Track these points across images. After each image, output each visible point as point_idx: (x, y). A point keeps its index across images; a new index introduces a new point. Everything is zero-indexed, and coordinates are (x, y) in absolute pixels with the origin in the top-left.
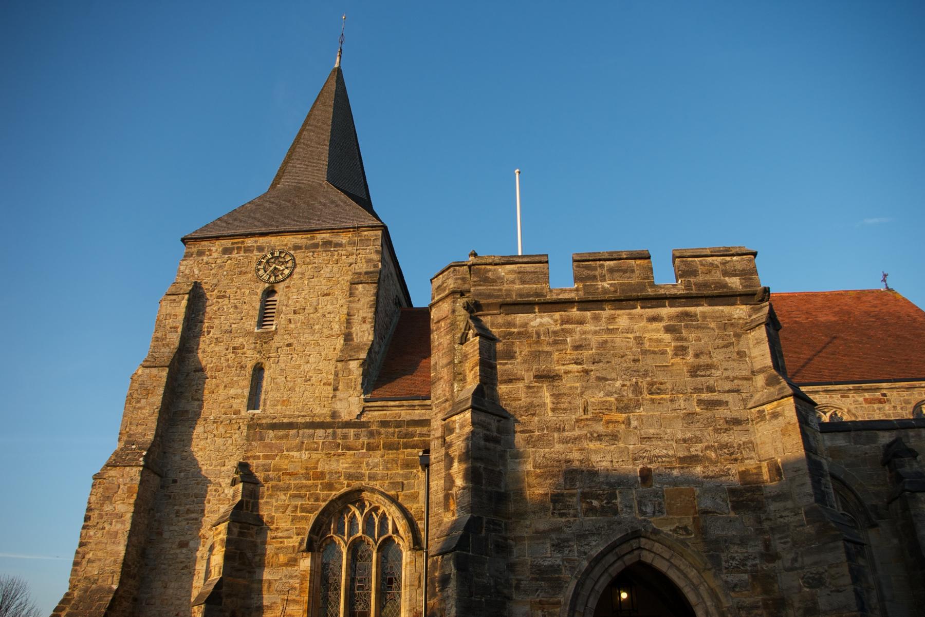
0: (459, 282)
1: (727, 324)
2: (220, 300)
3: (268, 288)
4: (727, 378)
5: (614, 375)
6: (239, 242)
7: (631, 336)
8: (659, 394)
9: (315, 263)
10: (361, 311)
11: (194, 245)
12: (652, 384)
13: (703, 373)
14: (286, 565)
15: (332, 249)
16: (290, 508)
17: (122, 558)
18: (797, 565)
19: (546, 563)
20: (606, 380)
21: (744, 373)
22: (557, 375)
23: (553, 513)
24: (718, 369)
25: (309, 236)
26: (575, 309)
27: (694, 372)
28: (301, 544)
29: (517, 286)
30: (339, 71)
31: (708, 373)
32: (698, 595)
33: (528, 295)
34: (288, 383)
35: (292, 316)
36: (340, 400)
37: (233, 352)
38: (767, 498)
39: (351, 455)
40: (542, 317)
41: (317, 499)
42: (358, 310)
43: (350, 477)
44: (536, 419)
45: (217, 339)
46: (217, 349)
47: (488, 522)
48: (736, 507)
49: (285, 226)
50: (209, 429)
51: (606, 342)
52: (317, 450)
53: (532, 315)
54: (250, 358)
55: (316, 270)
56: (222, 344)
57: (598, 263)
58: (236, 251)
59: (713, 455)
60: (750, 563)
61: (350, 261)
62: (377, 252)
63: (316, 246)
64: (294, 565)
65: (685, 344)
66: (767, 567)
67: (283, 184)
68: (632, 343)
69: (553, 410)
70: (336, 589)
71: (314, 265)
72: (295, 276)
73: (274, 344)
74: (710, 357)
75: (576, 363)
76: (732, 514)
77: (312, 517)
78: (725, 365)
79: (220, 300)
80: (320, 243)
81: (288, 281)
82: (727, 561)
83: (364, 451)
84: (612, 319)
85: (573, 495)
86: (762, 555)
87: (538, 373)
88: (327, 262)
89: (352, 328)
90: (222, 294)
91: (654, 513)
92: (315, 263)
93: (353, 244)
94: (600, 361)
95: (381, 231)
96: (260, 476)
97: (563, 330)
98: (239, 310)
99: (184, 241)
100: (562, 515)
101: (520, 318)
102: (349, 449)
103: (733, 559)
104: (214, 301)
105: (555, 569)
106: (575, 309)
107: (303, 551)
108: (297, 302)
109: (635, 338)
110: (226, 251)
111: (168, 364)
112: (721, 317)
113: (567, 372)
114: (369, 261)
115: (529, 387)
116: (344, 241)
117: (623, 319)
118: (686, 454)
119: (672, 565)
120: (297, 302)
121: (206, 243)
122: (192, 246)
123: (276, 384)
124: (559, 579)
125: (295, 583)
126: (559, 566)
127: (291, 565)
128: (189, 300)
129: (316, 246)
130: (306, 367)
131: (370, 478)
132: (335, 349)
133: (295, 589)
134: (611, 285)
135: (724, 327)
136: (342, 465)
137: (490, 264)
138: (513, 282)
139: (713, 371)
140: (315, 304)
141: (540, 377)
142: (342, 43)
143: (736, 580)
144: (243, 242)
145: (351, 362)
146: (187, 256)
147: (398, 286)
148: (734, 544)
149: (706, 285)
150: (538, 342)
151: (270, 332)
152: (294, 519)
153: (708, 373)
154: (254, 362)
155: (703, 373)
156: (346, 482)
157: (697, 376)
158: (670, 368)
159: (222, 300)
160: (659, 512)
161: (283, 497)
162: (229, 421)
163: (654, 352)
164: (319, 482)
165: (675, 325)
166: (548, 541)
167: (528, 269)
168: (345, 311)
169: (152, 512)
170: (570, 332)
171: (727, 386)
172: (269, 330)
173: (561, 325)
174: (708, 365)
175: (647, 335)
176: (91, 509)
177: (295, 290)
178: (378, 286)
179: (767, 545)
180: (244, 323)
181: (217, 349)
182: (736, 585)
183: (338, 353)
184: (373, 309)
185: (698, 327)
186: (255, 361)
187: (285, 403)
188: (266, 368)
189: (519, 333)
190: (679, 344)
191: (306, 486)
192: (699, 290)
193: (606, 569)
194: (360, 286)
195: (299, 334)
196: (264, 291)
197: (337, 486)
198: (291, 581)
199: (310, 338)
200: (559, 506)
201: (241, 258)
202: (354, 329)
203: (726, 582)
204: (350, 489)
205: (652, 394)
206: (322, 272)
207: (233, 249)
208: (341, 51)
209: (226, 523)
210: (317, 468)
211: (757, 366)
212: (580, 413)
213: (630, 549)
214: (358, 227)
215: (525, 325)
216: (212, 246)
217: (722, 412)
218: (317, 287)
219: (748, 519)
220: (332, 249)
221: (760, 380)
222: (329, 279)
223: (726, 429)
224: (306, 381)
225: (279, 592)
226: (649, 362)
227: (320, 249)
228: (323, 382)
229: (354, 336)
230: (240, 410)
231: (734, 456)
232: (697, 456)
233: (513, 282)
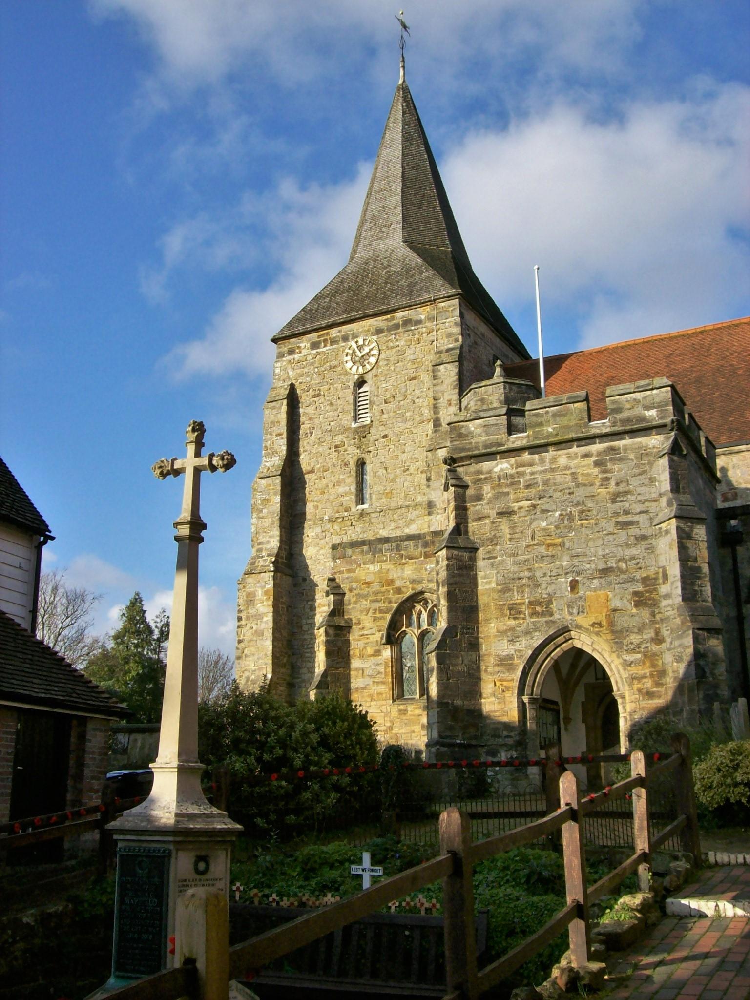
0: (479, 403)
1: (644, 454)
2: (316, 399)
3: (358, 379)
4: (640, 501)
5: (554, 507)
6: (324, 334)
8: (587, 519)
9: (398, 346)
10: (445, 394)
11: (284, 343)
12: (582, 512)
13: (621, 499)
14: (373, 655)
15: (413, 328)
17: (271, 652)
18: (672, 647)
19: (504, 654)
20: (548, 511)
21: (654, 496)
22: (513, 511)
23: (509, 618)
24: (633, 494)
25: (389, 316)
26: (527, 453)
27: (615, 497)
28: (382, 638)
29: (483, 439)
30: (405, 90)
31: (625, 498)
33: (491, 445)
34: (389, 475)
35: (384, 406)
36: (434, 490)
37: (335, 451)
38: (660, 596)
39: (412, 563)
40: (502, 464)
41: (390, 602)
42: (443, 392)
43: (413, 581)
44: (498, 548)
46: (321, 449)
47: (463, 628)
48: (636, 606)
49: (365, 310)
50: (326, 528)
51: (549, 480)
52: (386, 561)
53: (495, 462)
54: (352, 454)
55: (401, 353)
56: (324, 444)
57: (545, 410)
58: (323, 344)
59: (624, 566)
60: (643, 646)
61: (432, 338)
62: (456, 324)
63: (397, 326)
64: (379, 656)
65: (609, 475)
66: (655, 648)
67: (360, 254)
69: (510, 539)
71: (398, 348)
72: (381, 363)
73: (371, 438)
74: (628, 485)
75: (527, 500)
76: (634, 610)
77: (388, 617)
78: (639, 490)
79: (315, 399)
80: (401, 323)
81: (374, 370)
82: (627, 646)
83: (423, 558)
84: (554, 460)
85: (524, 603)
86: (652, 639)
87: (500, 511)
89: (439, 413)
90: (317, 392)
91: (578, 613)
92: (398, 346)
93: (431, 319)
95: (458, 300)
97: (517, 473)
98: (335, 407)
99: (275, 340)
100: (515, 619)
101: (486, 465)
102: (411, 558)
103: (632, 643)
104: (311, 400)
105: (510, 657)
106: (527, 453)
107: (384, 644)
108: (386, 390)
110: (315, 345)
111: (279, 472)
112: (640, 448)
113: (520, 508)
114: (449, 335)
115: (493, 523)
116: (423, 317)
117: (562, 457)
118: (604, 566)
120: (386, 390)
121: (294, 340)
122: (283, 346)
125: (381, 668)
126: (512, 655)
127: (377, 656)
128: (288, 405)
129: (397, 326)
130: (403, 457)
131: (429, 581)
132: (427, 434)
134: (554, 429)
135: (641, 457)
136: (409, 571)
137: (463, 421)
138: (480, 435)
139: (629, 496)
140: (404, 390)
141: (500, 514)
142: (402, 48)
143: (632, 659)
144: (328, 334)
145: (439, 451)
146: (281, 356)
148: (633, 633)
149: (628, 420)
150: (499, 485)
151: (366, 425)
153: (625, 498)
154: (355, 458)
155: (621, 499)
156: (411, 586)
157: (616, 502)
158: (596, 497)
159: (318, 398)
160: (582, 612)
161: (365, 603)
162: (341, 519)
163: (585, 485)
165: (602, 460)
166: (506, 638)
167: (491, 423)
168: (431, 394)
169: (290, 609)
170: (522, 474)
171: (638, 508)
172: (365, 423)
173: (516, 468)
174: (625, 492)
176: (241, 611)
177: (383, 379)
178: (460, 364)
179: (657, 632)
180: (341, 420)
181: (321, 449)
182: (632, 662)
183: (425, 442)
184: (457, 390)
185: (621, 459)
186: (356, 457)
187: (389, 495)
188: (368, 462)
189: (486, 479)
190: (605, 475)
192: (623, 426)
194: (442, 366)
195: (393, 423)
196: (355, 383)
197: (404, 590)
198: (378, 667)
200: (513, 612)
201: (329, 351)
202: (441, 413)
203: (625, 660)
204: (414, 592)
205: (582, 520)
206: (406, 355)
207: (319, 342)
208: (403, 61)
209: (324, 628)
211: (663, 491)
212: (529, 541)
213: (564, 640)
214: (435, 300)
215: (490, 472)
216: (300, 343)
217: (634, 531)
218: (403, 372)
219: (645, 614)
220: (413, 328)
223: (636, 544)
224: (404, 471)
225: (370, 676)
226: (581, 493)
227: (401, 330)
228: (420, 470)
229: (442, 420)
230: (350, 508)
231: (639, 566)
232: (612, 568)
233: (480, 435)
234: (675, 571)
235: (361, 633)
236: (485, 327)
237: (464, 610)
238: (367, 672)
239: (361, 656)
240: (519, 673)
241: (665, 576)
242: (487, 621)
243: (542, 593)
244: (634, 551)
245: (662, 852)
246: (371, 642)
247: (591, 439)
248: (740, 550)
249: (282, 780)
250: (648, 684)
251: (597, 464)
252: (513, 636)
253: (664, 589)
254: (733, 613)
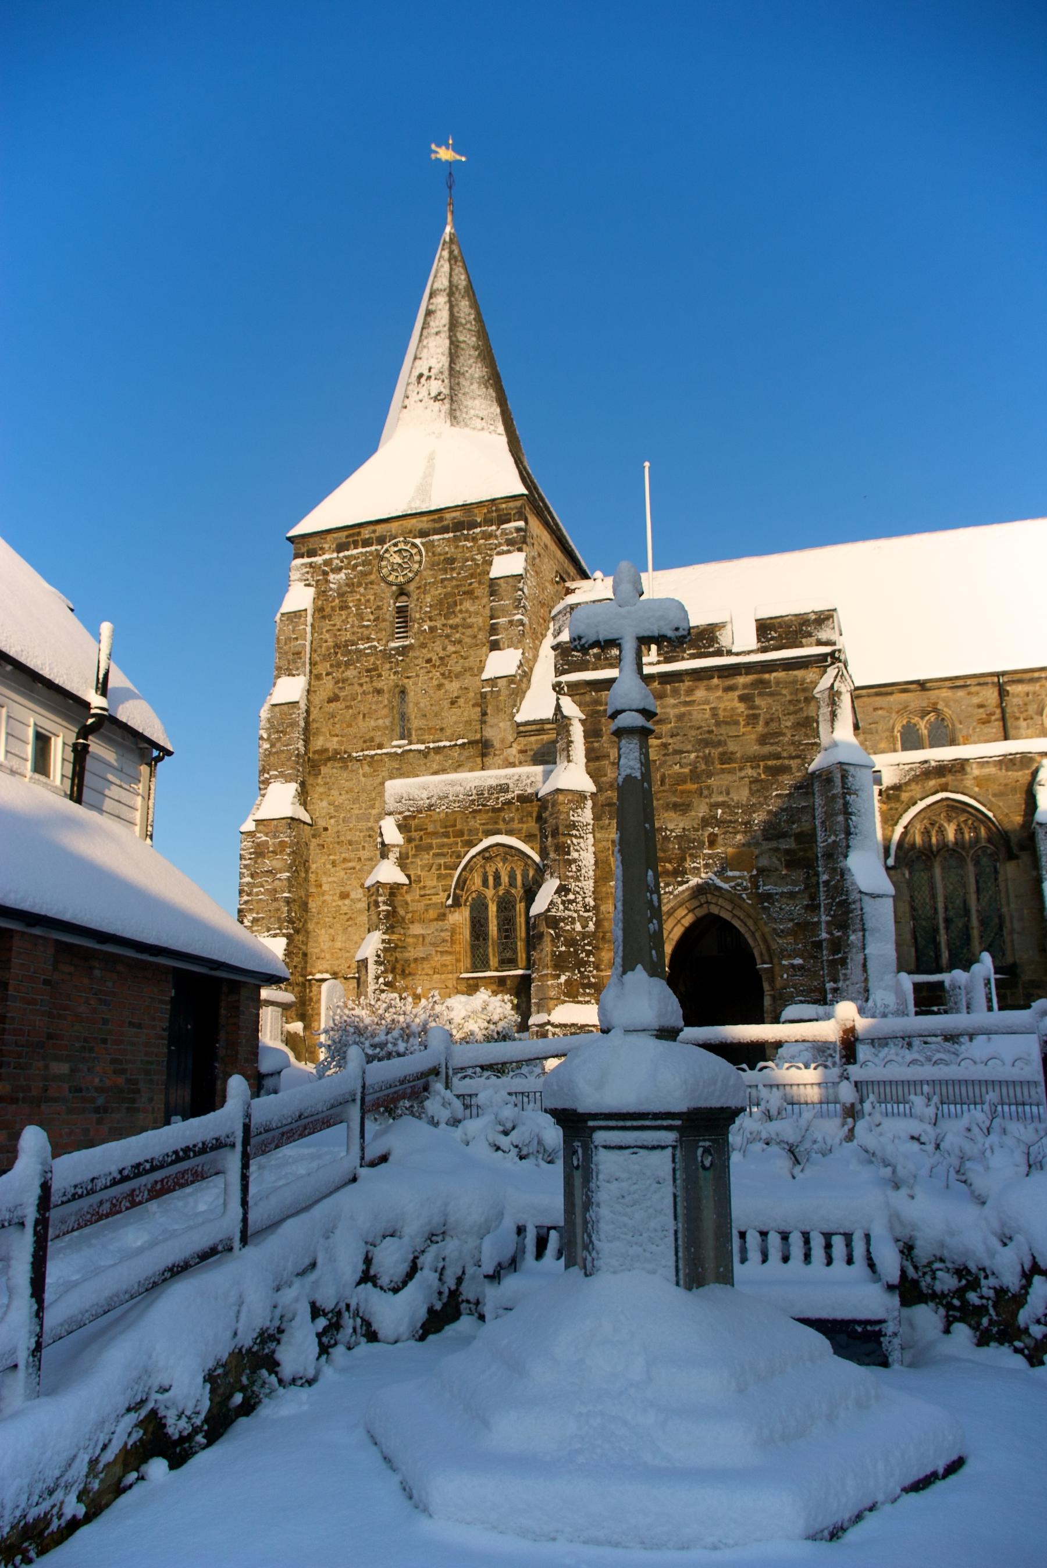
5: (689, 747)
7: (707, 707)
12: (724, 754)
14: (436, 920)
16: (434, 867)
25: (436, 517)
27: (763, 740)
32: (755, 940)
36: (492, 726)
48: (789, 865)
65: (757, 712)
70: (484, 939)
84: (690, 691)
94: (678, 734)
109: (711, 709)
112: (795, 682)
119: (735, 916)
133: (447, 941)
147: (559, 554)
152: (439, 877)
164: (459, 840)
175: (722, 706)
191: (448, 844)
193: (679, 921)
198: (442, 934)
210: (455, 826)
225: (432, 944)
235: (422, 893)
236: (548, 536)
238: (428, 940)
239: (422, 921)
246: (435, 904)
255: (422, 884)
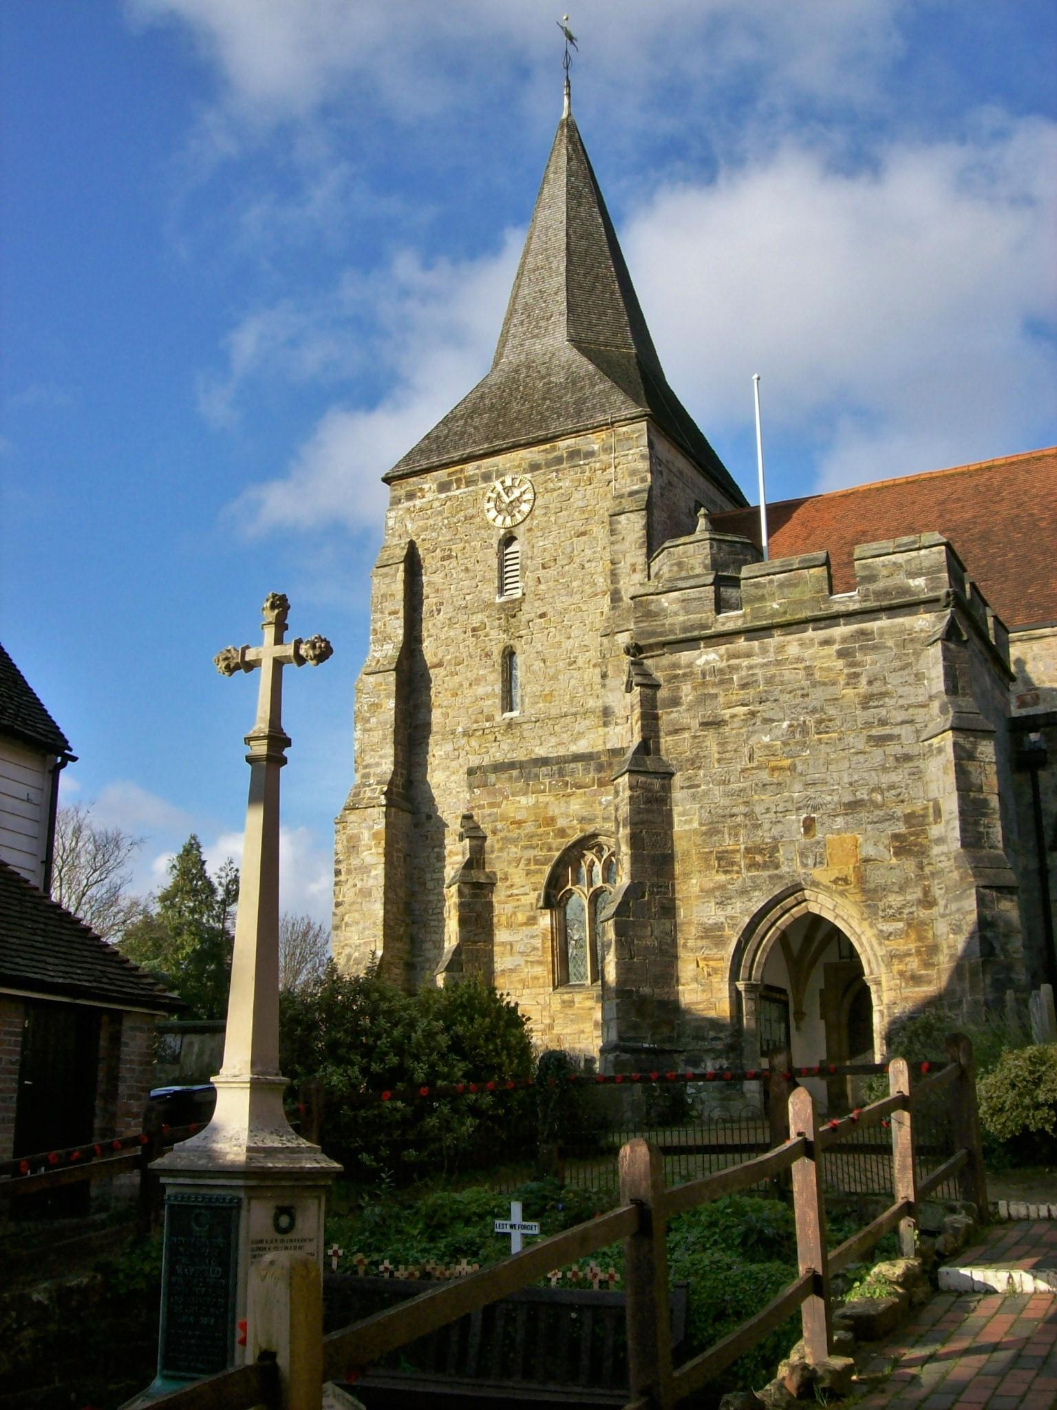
0: (675, 568)
1: (907, 640)
2: (446, 563)
3: (505, 534)
4: (902, 707)
5: (781, 715)
6: (457, 471)
8: (827, 732)
12: (820, 722)
13: (876, 703)
14: (525, 924)
15: (582, 463)
17: (382, 919)
19: (711, 922)
20: (773, 721)
21: (921, 699)
22: (723, 721)
23: (717, 871)
24: (892, 697)
25: (548, 446)
26: (743, 639)
27: (866, 701)
28: (538, 900)
29: (681, 618)
30: (571, 127)
31: (881, 703)
32: (861, 945)
33: (692, 628)
34: (548, 670)
35: (541, 573)
36: (611, 690)
37: (473, 636)
38: (930, 841)
39: (581, 794)
40: (707, 654)
41: (550, 849)
42: (624, 553)
43: (582, 820)
45: (450, 619)
46: (452, 633)
47: (653, 885)
48: (896, 854)
50: (459, 744)
51: (773, 676)
52: (543, 791)
53: (698, 652)
54: (496, 640)
55: (564, 498)
56: (457, 626)
57: (768, 578)
58: (455, 486)
59: (879, 798)
60: (906, 911)
61: (608, 477)
62: (642, 456)
63: (559, 460)
64: (534, 924)
65: (858, 670)
66: (923, 914)
67: (508, 358)
68: (802, 673)
69: (719, 761)
71: (560, 491)
72: (537, 512)
73: (523, 617)
74: (885, 683)
75: (742, 705)
76: (894, 861)
77: (547, 869)
78: (901, 691)
80: (565, 455)
81: (528, 521)
82: (883, 911)
83: (596, 787)
84: (781, 648)
86: (919, 902)
87: (705, 720)
88: (576, 484)
89: (619, 582)
90: (447, 553)
91: (815, 865)
92: (561, 488)
93: (607, 449)
95: (645, 423)
96: (486, 827)
97: (729, 666)
98: (472, 574)
99: (387, 480)
100: (726, 872)
101: (685, 656)
102: (579, 787)
103: (890, 907)
104: (439, 565)
105: (719, 927)
106: (743, 639)
107: (541, 908)
108: (545, 550)
110: (444, 487)
111: (393, 666)
112: (902, 632)
113: (733, 716)
114: (633, 473)
115: (695, 737)
116: (596, 447)
117: (793, 645)
118: (852, 799)
120: (545, 550)
121: (414, 479)
122: (399, 487)
123: (534, 672)
124: (721, 936)
125: (537, 942)
126: (722, 923)
127: (531, 924)
128: (406, 571)
129: (559, 460)
130: (568, 644)
132: (602, 613)
134: (780, 604)
135: (904, 644)
137: (652, 594)
138: (676, 614)
139: (887, 700)
140: (569, 550)
141: (705, 725)
142: (567, 68)
143: (891, 929)
144: (462, 471)
145: (619, 635)
146: (396, 501)
148: (893, 892)
149: (885, 593)
150: (704, 684)
151: (515, 600)
153: (881, 703)
154: (501, 646)
155: (876, 703)
156: (579, 826)
157: (868, 708)
158: (841, 701)
159: (448, 562)
160: (820, 863)
161: (514, 850)
163: (825, 684)
165: (848, 648)
166: (713, 900)
167: (693, 596)
168: (607, 556)
170: (736, 668)
171: (900, 716)
172: (514, 597)
173: (728, 660)
174: (881, 694)
176: (340, 862)
177: (540, 534)
178: (648, 514)
179: (926, 891)
180: (481, 592)
181: (452, 633)
182: (890, 934)
184: (644, 550)
186: (502, 644)
187: (549, 698)
188: (518, 652)
189: (684, 675)
190: (853, 670)
192: (878, 600)
194: (623, 517)
195: (553, 597)
196: (500, 540)
197: (569, 831)
198: (532, 941)
199: (567, 601)
200: (723, 863)
201: (464, 495)
202: (622, 582)
203: (881, 931)
204: (583, 834)
206: (572, 500)
207: (450, 483)
208: (569, 86)
209: (456, 885)
211: (934, 692)
213: (795, 902)
214: (613, 423)
215: (690, 665)
217: (893, 748)
219: (910, 865)
220: (582, 463)
221: (936, 705)
222: (582, 510)
223: (896, 768)
224: (570, 665)
225: (522, 953)
226: (818, 695)
228: (592, 663)
229: (623, 593)
230: (493, 716)
232: (862, 800)
233: (676, 614)
234: (951, 804)
235: (509, 893)
236: (684, 460)
237: (654, 860)
238: (517, 948)
239: (509, 926)
240: (731, 948)
241: (938, 813)
242: (687, 875)
243: (764, 836)
244: (894, 777)
245: (933, 1202)
246: (524, 906)
247: (833, 619)
248: (1044, 776)
249: (398, 1100)
250: (914, 964)
251: (841, 654)
252: (723, 897)
253: (935, 831)
254: (1033, 865)
255: (509, 883)
